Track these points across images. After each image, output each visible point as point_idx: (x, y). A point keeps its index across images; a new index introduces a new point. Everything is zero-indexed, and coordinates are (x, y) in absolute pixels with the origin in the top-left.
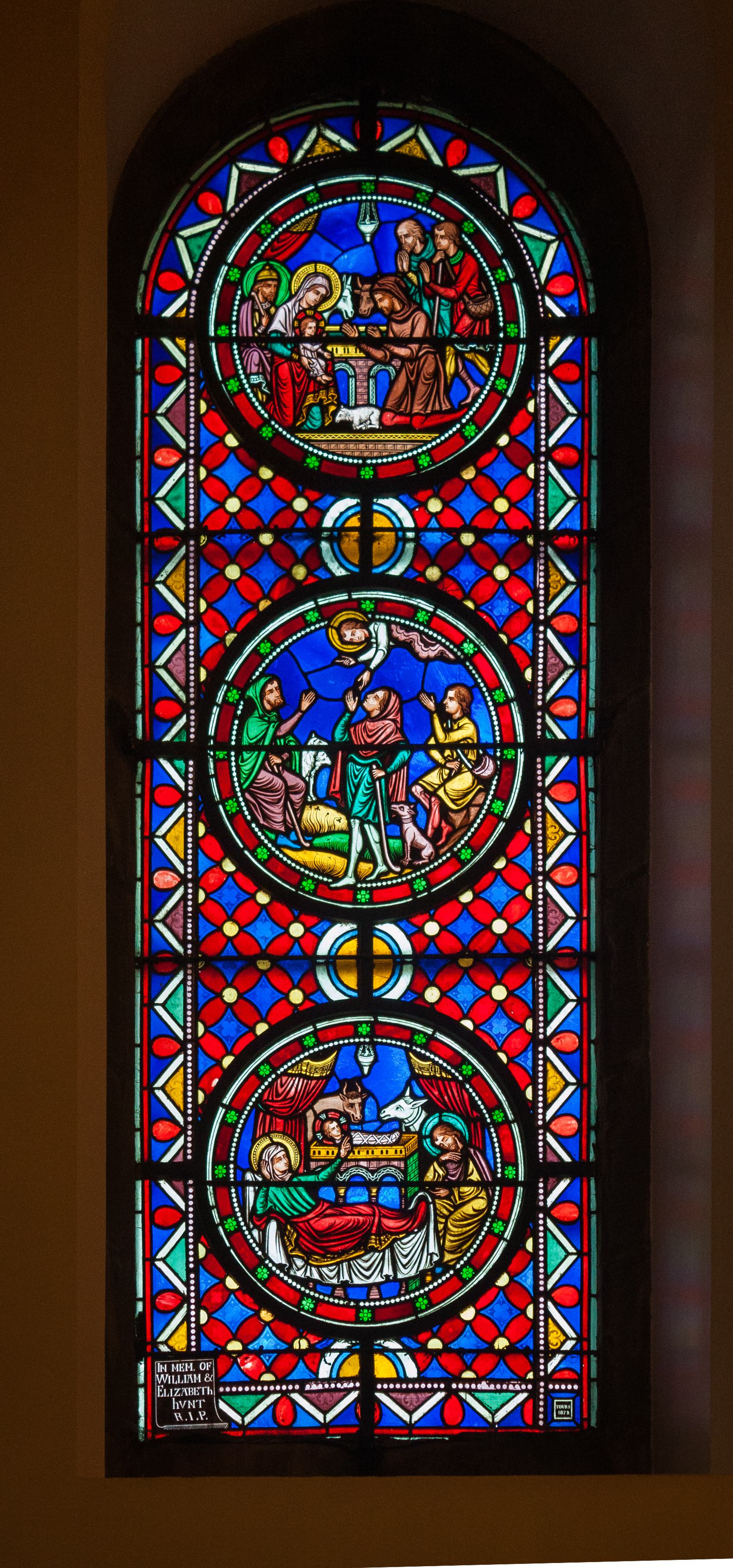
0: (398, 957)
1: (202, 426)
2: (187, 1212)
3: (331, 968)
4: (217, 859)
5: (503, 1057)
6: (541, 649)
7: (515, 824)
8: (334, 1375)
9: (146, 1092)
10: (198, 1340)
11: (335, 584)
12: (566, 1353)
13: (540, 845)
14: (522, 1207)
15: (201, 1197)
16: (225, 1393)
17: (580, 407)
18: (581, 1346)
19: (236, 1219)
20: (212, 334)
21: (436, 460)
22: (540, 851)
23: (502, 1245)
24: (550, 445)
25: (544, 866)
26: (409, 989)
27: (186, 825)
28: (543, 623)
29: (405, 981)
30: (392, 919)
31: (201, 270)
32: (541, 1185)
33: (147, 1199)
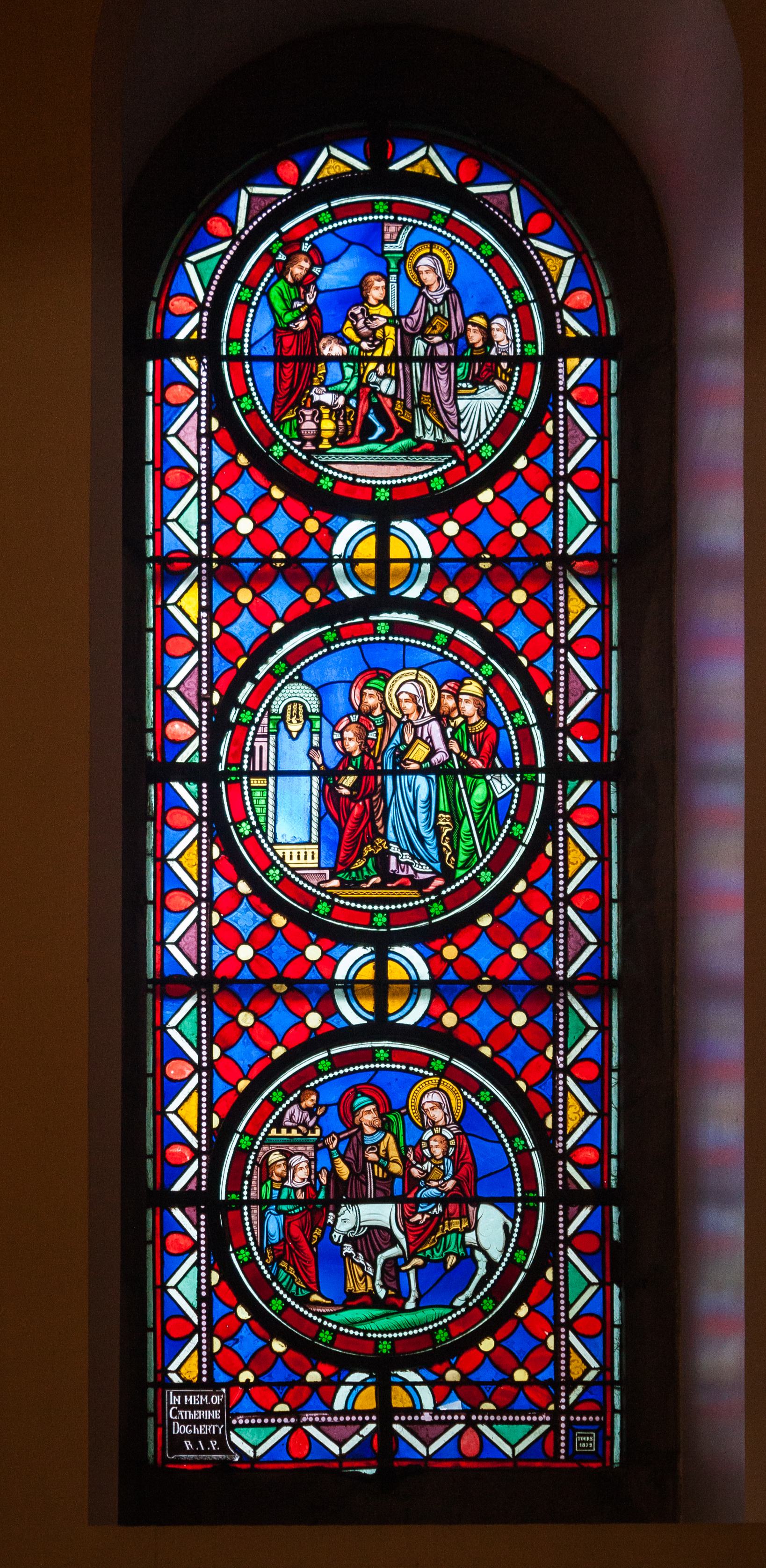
0: (415, 981)
1: (215, 1366)
2: (200, 389)
3: (349, 991)
5: (522, 1085)
6: (561, 1094)
7: (536, 1271)
8: (349, 1407)
9: (159, 692)
10: (210, 1369)
11: (352, 1033)
12: (587, 1385)
13: (561, 870)
14: (541, 389)
15: (215, 795)
16: (238, 1425)
17: (599, 515)
18: (604, 1376)
20: (224, 352)
21: (453, 1334)
22: (562, 1302)
23: (521, 850)
24: (571, 1316)
26: (427, 1014)
27: (199, 421)
28: (563, 478)
31: (211, 293)
32: (560, 786)
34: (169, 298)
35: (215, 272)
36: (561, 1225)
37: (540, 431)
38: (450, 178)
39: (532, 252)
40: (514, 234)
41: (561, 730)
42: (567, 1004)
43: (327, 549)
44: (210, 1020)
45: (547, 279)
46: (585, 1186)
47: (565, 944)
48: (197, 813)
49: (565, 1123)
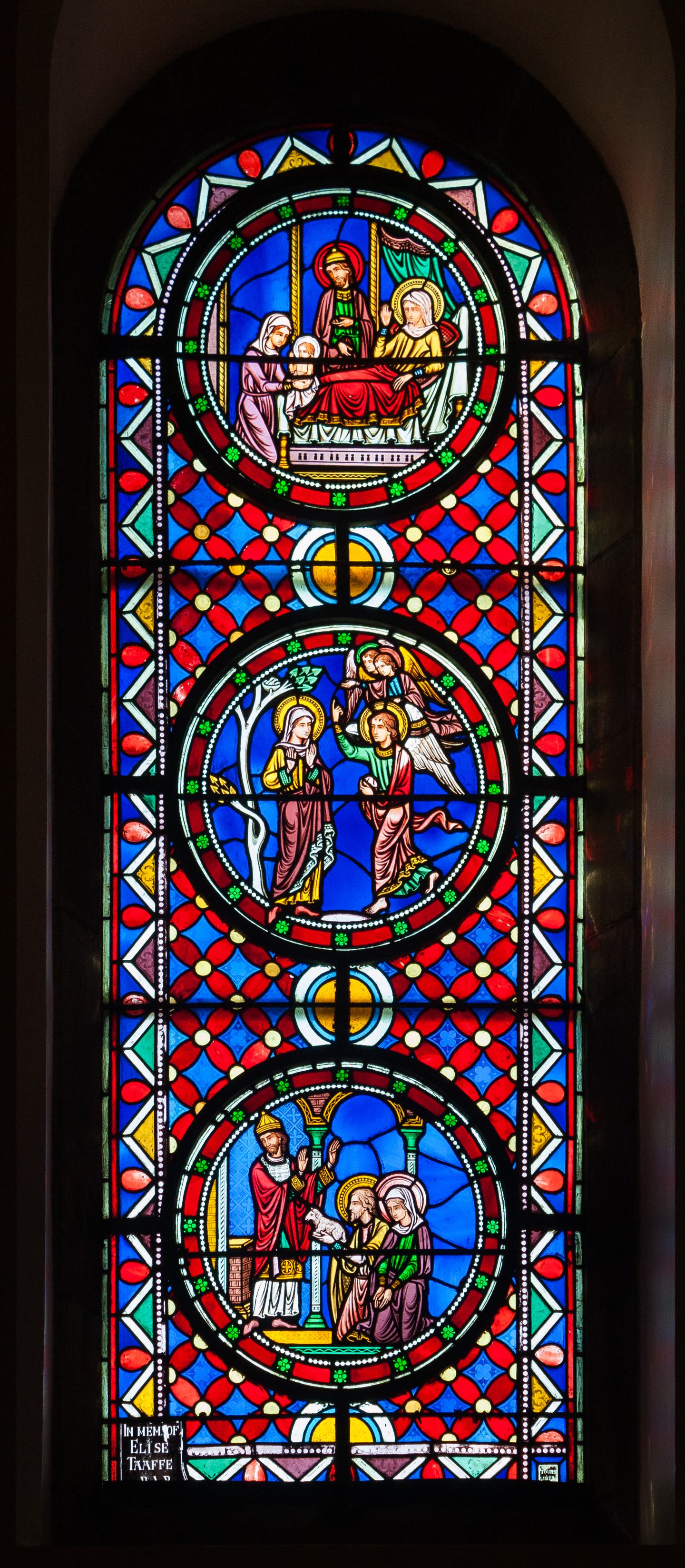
2: (156, 475)
4: (191, 897)
8: (307, 1440)
11: (313, 1055)
12: (550, 1416)
19: (209, 835)
25: (530, 1082)
26: (389, 1032)
29: (384, 1024)
30: (373, 522)
32: (524, 367)
33: (114, 635)
34: (127, 288)
35: (174, 266)
36: (524, 1249)
37: (504, 870)
38: (413, 174)
39: (496, 251)
40: (479, 231)
41: (527, 832)
42: (531, 1025)
43: (286, 1433)
44: (166, 604)
45: (511, 280)
46: (548, 1210)
47: (530, 964)
48: (154, 910)
49: (529, 1145)
